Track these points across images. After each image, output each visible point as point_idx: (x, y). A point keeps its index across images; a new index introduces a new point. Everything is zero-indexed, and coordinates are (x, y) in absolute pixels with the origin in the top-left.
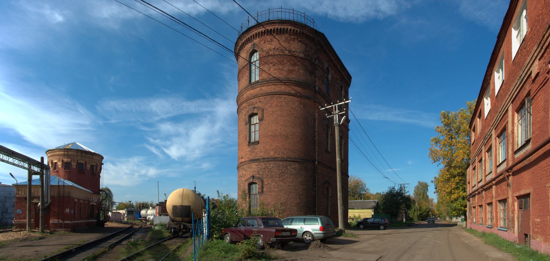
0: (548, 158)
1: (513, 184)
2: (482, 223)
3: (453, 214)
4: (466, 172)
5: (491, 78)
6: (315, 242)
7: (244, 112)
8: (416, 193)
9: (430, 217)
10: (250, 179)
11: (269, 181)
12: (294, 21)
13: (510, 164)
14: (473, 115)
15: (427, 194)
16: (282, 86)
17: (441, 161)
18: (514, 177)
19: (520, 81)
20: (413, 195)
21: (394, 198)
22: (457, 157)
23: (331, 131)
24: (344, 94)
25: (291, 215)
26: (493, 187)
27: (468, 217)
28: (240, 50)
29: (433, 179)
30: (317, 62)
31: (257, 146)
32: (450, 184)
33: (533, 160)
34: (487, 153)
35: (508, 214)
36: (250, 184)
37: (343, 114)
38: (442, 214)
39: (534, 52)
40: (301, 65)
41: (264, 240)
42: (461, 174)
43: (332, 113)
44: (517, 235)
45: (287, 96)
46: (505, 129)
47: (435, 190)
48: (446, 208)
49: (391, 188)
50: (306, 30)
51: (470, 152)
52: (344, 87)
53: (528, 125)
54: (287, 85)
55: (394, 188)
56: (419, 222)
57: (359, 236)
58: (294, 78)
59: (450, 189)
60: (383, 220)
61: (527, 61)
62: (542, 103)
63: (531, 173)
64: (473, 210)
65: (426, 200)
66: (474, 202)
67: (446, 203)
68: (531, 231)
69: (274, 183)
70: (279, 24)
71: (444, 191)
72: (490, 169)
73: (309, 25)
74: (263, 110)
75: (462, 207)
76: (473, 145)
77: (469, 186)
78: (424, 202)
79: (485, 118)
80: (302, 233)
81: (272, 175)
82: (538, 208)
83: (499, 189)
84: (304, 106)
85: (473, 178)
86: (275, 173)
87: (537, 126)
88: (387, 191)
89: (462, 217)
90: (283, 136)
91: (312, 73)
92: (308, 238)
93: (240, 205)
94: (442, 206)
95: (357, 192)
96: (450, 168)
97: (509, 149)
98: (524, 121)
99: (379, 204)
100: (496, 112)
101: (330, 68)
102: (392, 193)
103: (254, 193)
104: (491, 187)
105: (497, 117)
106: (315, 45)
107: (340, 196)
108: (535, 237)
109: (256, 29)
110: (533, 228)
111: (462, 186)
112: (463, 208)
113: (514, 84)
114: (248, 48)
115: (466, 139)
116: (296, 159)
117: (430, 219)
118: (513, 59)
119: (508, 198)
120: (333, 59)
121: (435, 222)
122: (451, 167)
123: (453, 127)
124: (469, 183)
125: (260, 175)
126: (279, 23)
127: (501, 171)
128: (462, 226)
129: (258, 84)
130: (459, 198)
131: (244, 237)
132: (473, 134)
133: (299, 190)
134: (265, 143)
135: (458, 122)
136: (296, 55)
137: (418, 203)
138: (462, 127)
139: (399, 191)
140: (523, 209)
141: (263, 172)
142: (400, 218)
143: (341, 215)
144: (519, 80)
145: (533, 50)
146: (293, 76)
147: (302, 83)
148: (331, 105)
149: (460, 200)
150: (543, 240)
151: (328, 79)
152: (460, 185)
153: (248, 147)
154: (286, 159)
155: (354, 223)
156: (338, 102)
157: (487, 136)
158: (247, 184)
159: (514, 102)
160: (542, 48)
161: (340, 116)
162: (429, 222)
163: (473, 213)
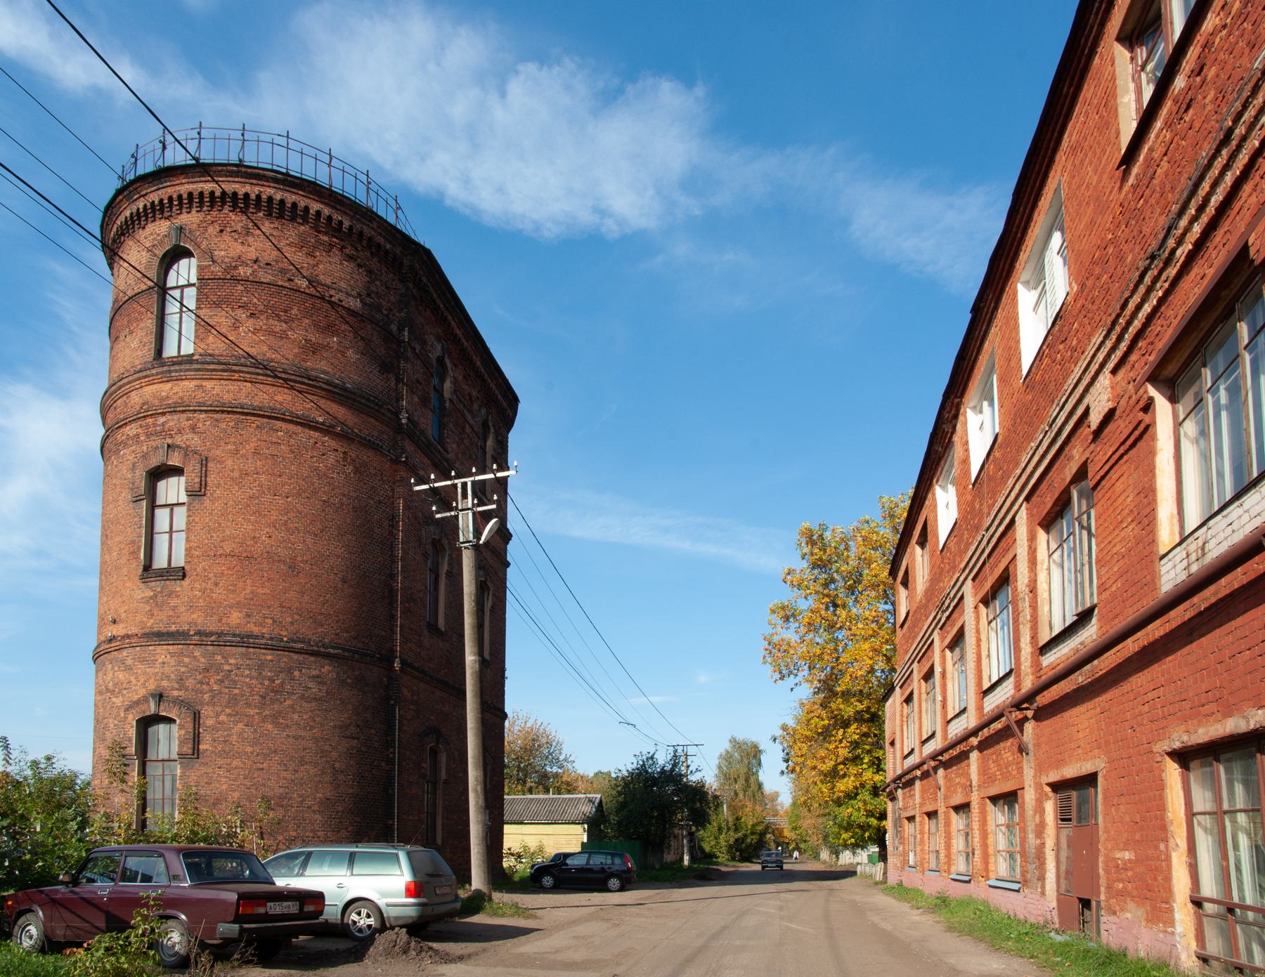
0: (1156, 665)
1: (1037, 745)
2: (937, 867)
3: (841, 841)
4: (884, 711)
5: (954, 427)
6: (389, 935)
7: (128, 454)
8: (726, 776)
9: (770, 850)
10: (148, 702)
11: (223, 718)
12: (330, 190)
13: (1028, 684)
14: (902, 535)
15: (757, 780)
16: (280, 389)
17: (800, 674)
18: (1039, 723)
19: (1051, 435)
20: (713, 779)
21: (652, 791)
22: (852, 663)
23: (450, 564)
24: (494, 450)
25: (304, 841)
26: (971, 755)
27: (890, 848)
28: (123, 234)
29: (779, 733)
30: (406, 333)
31: (177, 586)
32: (832, 747)
33: (1104, 671)
34: (948, 652)
35: (1024, 840)
36: (146, 723)
37: (489, 510)
38: (805, 841)
39: (1093, 350)
40: (351, 335)
41: (189, 931)
42: (867, 716)
43: (454, 505)
44: (1054, 904)
45: (299, 429)
46: (1005, 579)
47: (785, 765)
48: (820, 820)
49: (644, 758)
50: (373, 228)
51: (895, 650)
52: (494, 426)
53: (1083, 565)
54: (300, 392)
55: (652, 758)
56: (734, 866)
57: (539, 913)
58: (324, 372)
59: (833, 763)
60: (617, 861)
61: (1072, 377)
62: (1129, 499)
63: (1098, 710)
64: (908, 828)
65: (754, 796)
66: (911, 801)
67: (820, 805)
68: (1102, 889)
69: (240, 725)
70: (278, 184)
71: (814, 768)
72: (959, 702)
73: (381, 213)
74: (204, 462)
75: (872, 819)
76: (902, 626)
77: (894, 753)
78: (748, 804)
79: (941, 547)
80: (341, 905)
81: (235, 695)
82: (1127, 819)
83: (991, 762)
84: (357, 471)
85: (905, 728)
86: (245, 688)
87: (1116, 569)
88: (630, 767)
89: (872, 850)
90: (279, 561)
91: (386, 367)
92: (363, 920)
93: (99, 801)
94: (807, 813)
95: (534, 768)
96: (830, 697)
97: (1022, 640)
98: (1069, 556)
99: (604, 805)
100: (977, 528)
101: (447, 361)
102: (647, 772)
103: (160, 758)
104: (964, 756)
105: (980, 542)
106: (401, 281)
107: (476, 780)
108: (1118, 908)
109: (191, 180)
110: (1108, 879)
111: (869, 752)
112: (874, 822)
113: (1033, 444)
114: (158, 235)
115: (880, 610)
116: (323, 646)
117: (769, 855)
118: (1025, 371)
119: (1023, 788)
120: (458, 332)
121: (785, 867)
122: (832, 694)
123: (837, 571)
124: (892, 743)
125: (187, 690)
126: (276, 181)
127: (997, 707)
128: (871, 876)
129: (187, 367)
130: (860, 791)
131: (107, 921)
132: (902, 593)
133: (334, 754)
134: (210, 579)
135: (853, 558)
136: (333, 299)
137: (729, 807)
138: (866, 571)
139: (668, 767)
140: (1074, 822)
141: (201, 683)
142: (672, 852)
143: (479, 844)
144: (1046, 432)
145: (1092, 344)
146: (323, 365)
147: (351, 392)
148: (450, 478)
149: (865, 795)
150: (1145, 916)
151: (442, 395)
152: (864, 749)
153: (142, 586)
154: (287, 642)
155: (523, 869)
156: (474, 470)
157: (948, 601)
158: (132, 719)
159: (1034, 499)
160: (1120, 339)
161: (478, 515)
162: (767, 867)
163: (906, 836)
